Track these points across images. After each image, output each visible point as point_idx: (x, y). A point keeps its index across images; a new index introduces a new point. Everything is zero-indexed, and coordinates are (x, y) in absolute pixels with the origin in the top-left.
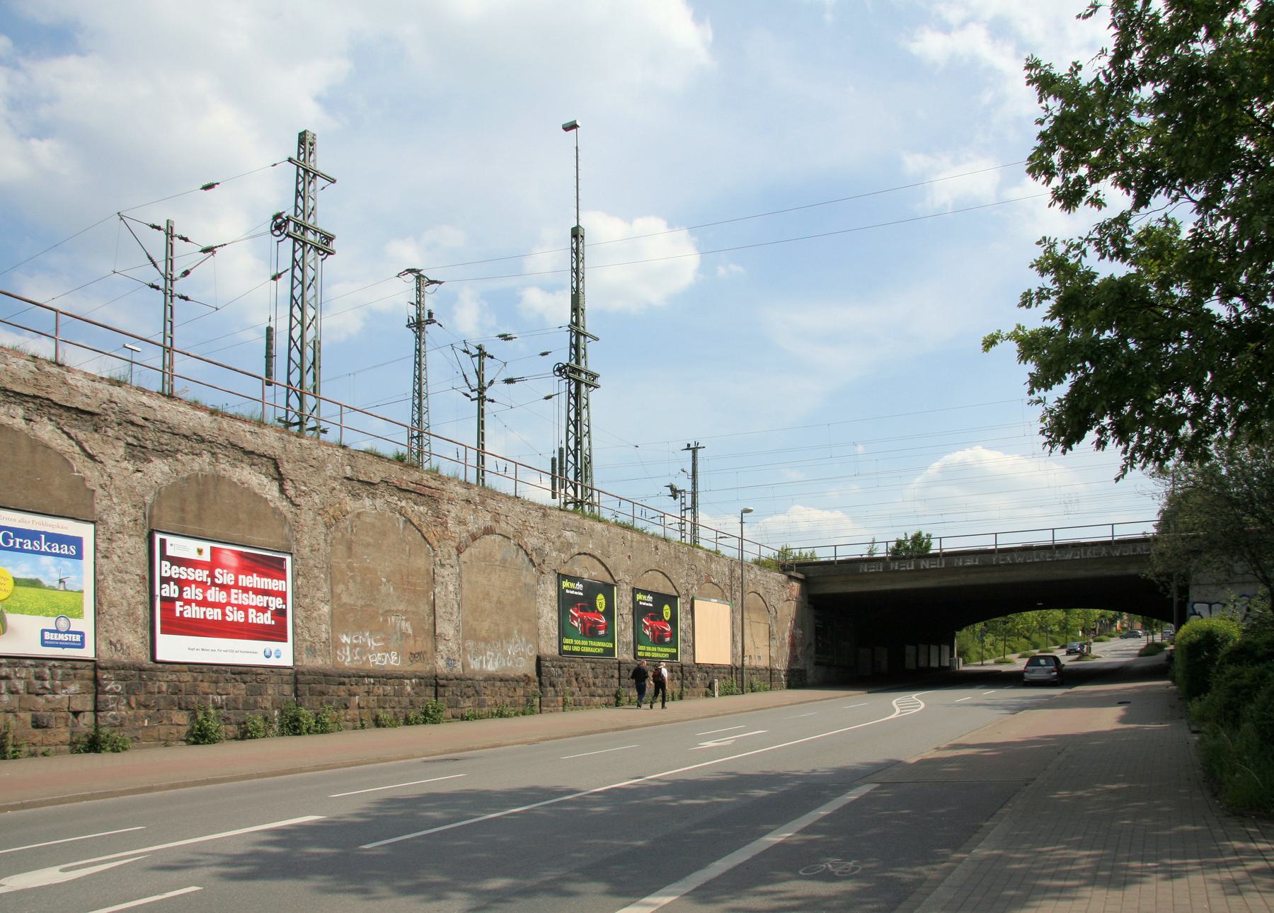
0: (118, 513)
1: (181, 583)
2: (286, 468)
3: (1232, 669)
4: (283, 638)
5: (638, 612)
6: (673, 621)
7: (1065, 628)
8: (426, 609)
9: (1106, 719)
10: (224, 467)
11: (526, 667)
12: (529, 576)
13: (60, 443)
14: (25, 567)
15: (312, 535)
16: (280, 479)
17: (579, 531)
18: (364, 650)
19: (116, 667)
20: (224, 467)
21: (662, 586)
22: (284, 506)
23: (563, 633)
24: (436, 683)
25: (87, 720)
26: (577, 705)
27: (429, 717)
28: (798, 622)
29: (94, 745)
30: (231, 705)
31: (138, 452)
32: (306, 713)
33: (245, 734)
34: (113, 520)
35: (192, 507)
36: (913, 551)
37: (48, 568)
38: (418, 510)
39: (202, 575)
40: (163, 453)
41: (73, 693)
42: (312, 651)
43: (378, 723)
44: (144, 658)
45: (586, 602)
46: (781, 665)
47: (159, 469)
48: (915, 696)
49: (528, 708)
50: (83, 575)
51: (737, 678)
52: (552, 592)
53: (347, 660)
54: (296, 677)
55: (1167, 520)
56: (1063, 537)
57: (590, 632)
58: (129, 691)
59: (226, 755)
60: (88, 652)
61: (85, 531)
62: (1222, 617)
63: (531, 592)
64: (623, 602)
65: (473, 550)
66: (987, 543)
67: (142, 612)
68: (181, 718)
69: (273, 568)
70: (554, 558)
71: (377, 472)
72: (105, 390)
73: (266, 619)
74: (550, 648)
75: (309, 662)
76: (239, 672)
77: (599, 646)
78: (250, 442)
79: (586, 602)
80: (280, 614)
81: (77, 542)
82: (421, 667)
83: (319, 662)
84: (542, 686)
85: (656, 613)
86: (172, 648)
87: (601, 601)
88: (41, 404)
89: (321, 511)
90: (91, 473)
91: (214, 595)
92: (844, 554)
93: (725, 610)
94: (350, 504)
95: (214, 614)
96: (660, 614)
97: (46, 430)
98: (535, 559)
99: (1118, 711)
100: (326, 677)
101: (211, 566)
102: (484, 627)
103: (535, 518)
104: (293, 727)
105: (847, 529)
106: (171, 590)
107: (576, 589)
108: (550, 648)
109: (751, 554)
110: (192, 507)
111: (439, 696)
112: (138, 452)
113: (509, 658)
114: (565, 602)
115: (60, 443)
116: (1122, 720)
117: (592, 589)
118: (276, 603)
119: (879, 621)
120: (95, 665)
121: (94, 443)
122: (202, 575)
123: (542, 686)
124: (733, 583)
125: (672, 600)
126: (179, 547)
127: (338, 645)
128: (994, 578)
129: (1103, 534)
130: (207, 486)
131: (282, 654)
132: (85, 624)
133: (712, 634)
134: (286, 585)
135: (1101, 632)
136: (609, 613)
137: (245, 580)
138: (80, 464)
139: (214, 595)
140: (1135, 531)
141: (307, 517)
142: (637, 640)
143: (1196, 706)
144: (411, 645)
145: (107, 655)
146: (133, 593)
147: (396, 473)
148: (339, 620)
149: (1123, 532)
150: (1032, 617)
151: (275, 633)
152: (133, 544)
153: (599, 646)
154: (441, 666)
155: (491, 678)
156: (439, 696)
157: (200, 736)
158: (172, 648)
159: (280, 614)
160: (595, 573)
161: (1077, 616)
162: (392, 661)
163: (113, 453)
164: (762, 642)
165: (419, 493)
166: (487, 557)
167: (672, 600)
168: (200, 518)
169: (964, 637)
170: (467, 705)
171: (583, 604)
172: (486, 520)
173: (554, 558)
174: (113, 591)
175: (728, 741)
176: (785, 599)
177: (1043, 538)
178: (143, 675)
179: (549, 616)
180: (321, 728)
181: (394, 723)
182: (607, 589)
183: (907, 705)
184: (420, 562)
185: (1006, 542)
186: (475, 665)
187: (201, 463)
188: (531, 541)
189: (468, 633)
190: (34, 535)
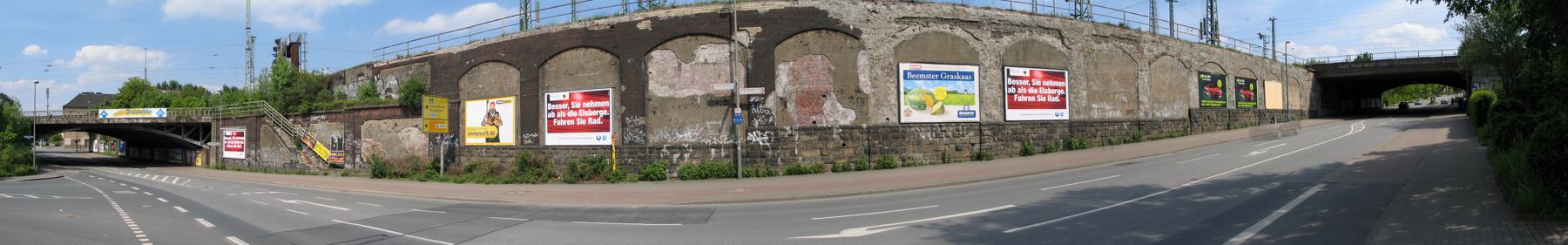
0: (989, 60)
1: (1016, 87)
2: (1064, 33)
3: (1497, 115)
4: (1064, 107)
5: (1238, 87)
6: (1255, 91)
7: (1425, 92)
8: (1133, 90)
9: (1438, 136)
10: (1036, 36)
11: (1184, 114)
12: (1184, 73)
13: (964, 35)
14: (951, 86)
15: (1078, 61)
16: (1062, 38)
17: (1208, 52)
18: (1104, 110)
19: (989, 124)
20: (1036, 36)
21: (1249, 75)
22: (1064, 50)
23: (1201, 98)
24: (1139, 124)
25: (977, 147)
26: (1209, 130)
27: (1136, 139)
28: (1313, 90)
29: (979, 157)
30: (1040, 138)
31: (997, 34)
32: (1075, 141)
33: (1047, 151)
34: (987, 63)
35: (1021, 54)
36: (1364, 60)
37: (960, 86)
38: (1129, 47)
39: (1026, 82)
40: (1008, 33)
41: (971, 136)
42: (1078, 112)
43: (1111, 143)
44: (1001, 120)
45: (1213, 83)
46: (1306, 109)
47: (1006, 40)
48: (1362, 122)
49: (1185, 133)
50: (974, 87)
51: (1284, 115)
52: (1196, 80)
53: (1096, 115)
54: (1070, 124)
55: (1462, 50)
56: (1422, 55)
57: (1215, 97)
58: (995, 134)
59: (1038, 161)
60: (977, 119)
61: (975, 69)
62: (1485, 89)
63: (1186, 81)
64: (1230, 83)
65: (1158, 62)
66: (1392, 56)
67: (1000, 100)
68: (1017, 145)
69: (1060, 77)
70: (1196, 65)
71: (1108, 32)
72: (981, 12)
73: (1056, 99)
74: (1195, 105)
75: (1076, 117)
76: (1044, 123)
77: (1219, 103)
78: (1047, 24)
79: (1213, 83)
80: (1063, 96)
81: (972, 74)
82: (1132, 117)
83: (1082, 117)
84: (1191, 123)
85: (1247, 87)
86: (1013, 115)
87: (1219, 83)
88: (955, 22)
89: (1082, 50)
90: (977, 46)
91: (1031, 91)
92: (1332, 61)
93: (1279, 85)
94: (1096, 46)
95: (1032, 99)
96: (1249, 88)
97: (958, 32)
98: (1187, 66)
99: (1445, 131)
100: (1084, 123)
101: (1030, 79)
102: (1162, 97)
103: (1187, 47)
104: (1069, 147)
105: (1337, 49)
106: (1012, 90)
107: (1208, 78)
108: (1195, 105)
109: (1291, 61)
110: (1021, 54)
111: (1140, 130)
112: (997, 34)
113: (1178, 110)
114: (1202, 84)
115: (964, 35)
116: (1449, 136)
117: (1215, 78)
118: (1061, 92)
119: (1347, 90)
120: (980, 124)
121: (977, 33)
122: (1026, 82)
123: (1191, 123)
124: (1284, 74)
125: (1254, 82)
126: (1015, 71)
127: (1091, 109)
128: (1410, 70)
129: (1438, 54)
130: (1027, 46)
131: (1064, 115)
132: (976, 107)
133: (1273, 96)
134: (1066, 84)
135: (1438, 93)
136: (1224, 88)
137: (1046, 83)
138: (973, 43)
139: (1031, 91)
140: (1451, 53)
141: (1075, 54)
142: (1238, 100)
143: (1482, 131)
144: (1127, 107)
145: (985, 119)
146: (995, 93)
147: (1118, 32)
148: (1092, 97)
149: (1446, 54)
150: (1412, 87)
151: (1061, 105)
152: (996, 72)
153: (1219, 103)
154: (1142, 115)
155: (1166, 120)
156: (1140, 130)
157: (1026, 152)
158: (1013, 115)
159: (1063, 96)
160: (1218, 71)
161: (1429, 87)
162: (1118, 115)
163: (986, 36)
164: (1297, 98)
165: (1129, 39)
166: (1164, 66)
167: (1254, 82)
168: (1025, 59)
169: (1385, 95)
170: (1155, 133)
171: (1211, 85)
172: (1163, 49)
173: (1196, 65)
174: (987, 93)
175: (1264, 151)
176: (1307, 80)
177: (1415, 55)
178: (997, 126)
179: (1194, 90)
180: (1082, 147)
181: (1118, 143)
182: (1223, 78)
183: (1358, 126)
184: (1131, 70)
185: (1399, 56)
186: (1158, 115)
187: (1026, 35)
188: (1185, 58)
189: (1154, 100)
190: (954, 73)
